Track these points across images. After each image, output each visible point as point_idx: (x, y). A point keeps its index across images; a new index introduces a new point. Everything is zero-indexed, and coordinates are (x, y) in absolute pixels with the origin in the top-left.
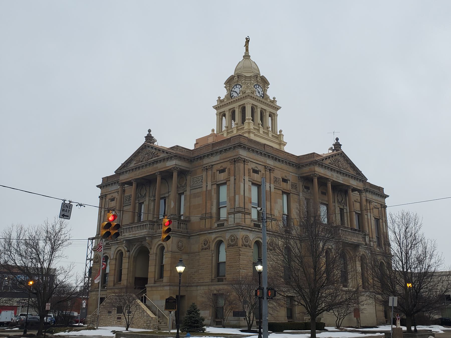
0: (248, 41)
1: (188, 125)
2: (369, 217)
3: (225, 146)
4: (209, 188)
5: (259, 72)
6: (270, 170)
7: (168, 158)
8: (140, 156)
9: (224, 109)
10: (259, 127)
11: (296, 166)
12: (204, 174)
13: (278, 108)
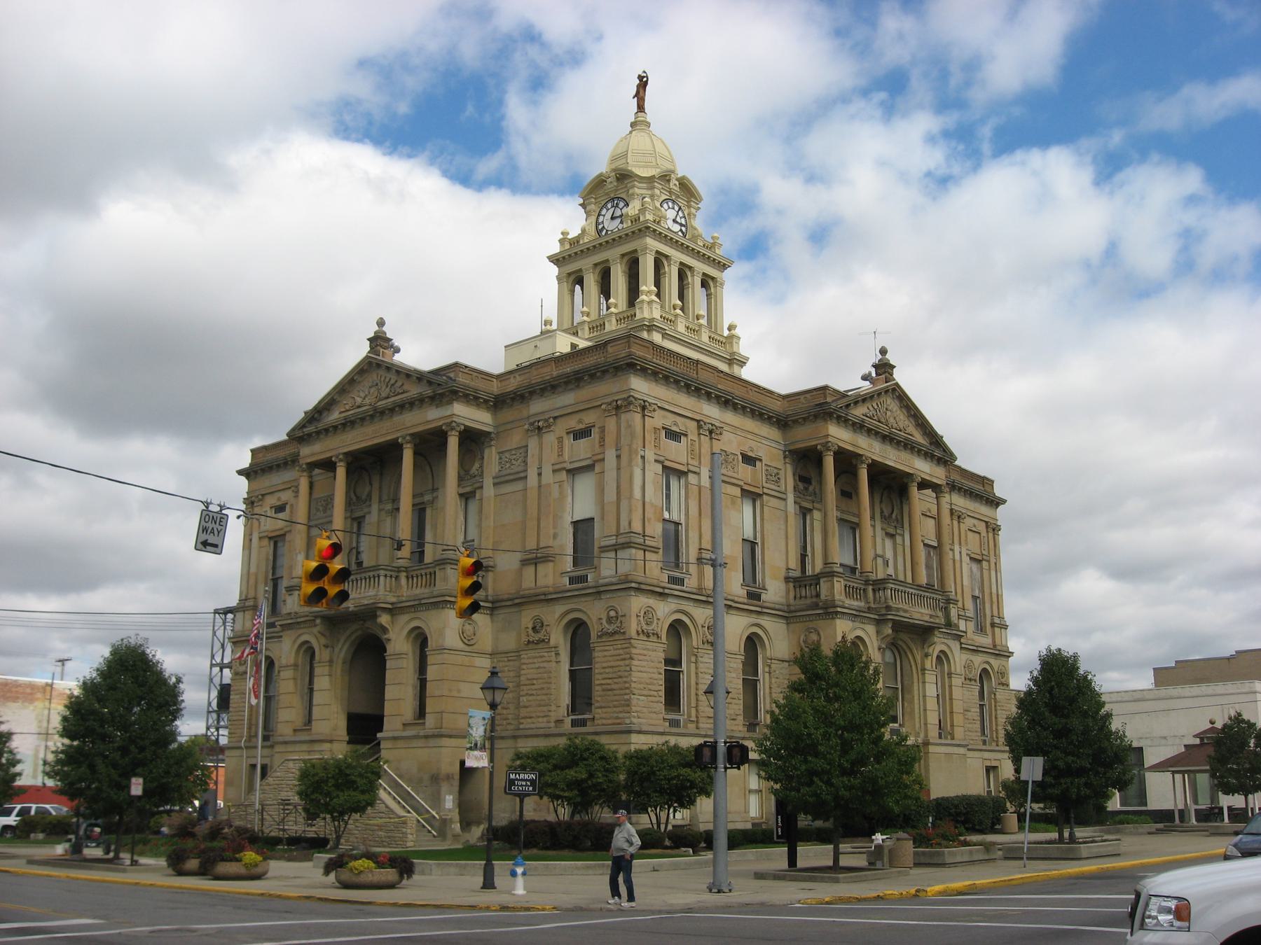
0: (643, 83)
2: (957, 557)
12: (533, 443)
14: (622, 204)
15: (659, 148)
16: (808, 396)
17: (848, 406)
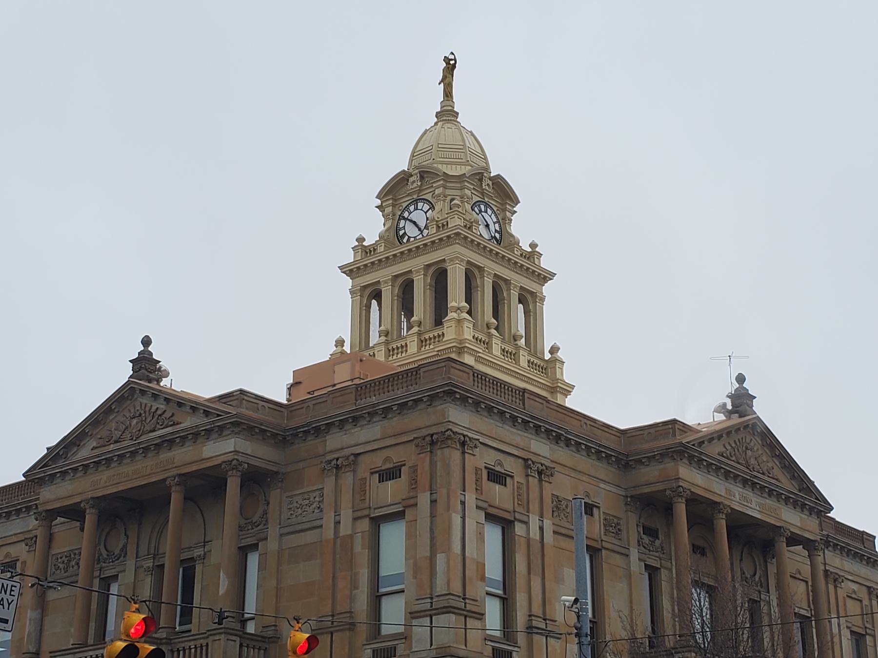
0: (450, 66)
1: (266, 328)
3: (399, 393)
4: (345, 529)
5: (487, 163)
6: (540, 473)
7: (208, 432)
8: (112, 424)
9: (379, 278)
10: (490, 335)
11: (618, 460)
12: (329, 483)
13: (544, 277)
14: (426, 207)
15: (470, 142)
16: (652, 431)
17: (701, 443)
